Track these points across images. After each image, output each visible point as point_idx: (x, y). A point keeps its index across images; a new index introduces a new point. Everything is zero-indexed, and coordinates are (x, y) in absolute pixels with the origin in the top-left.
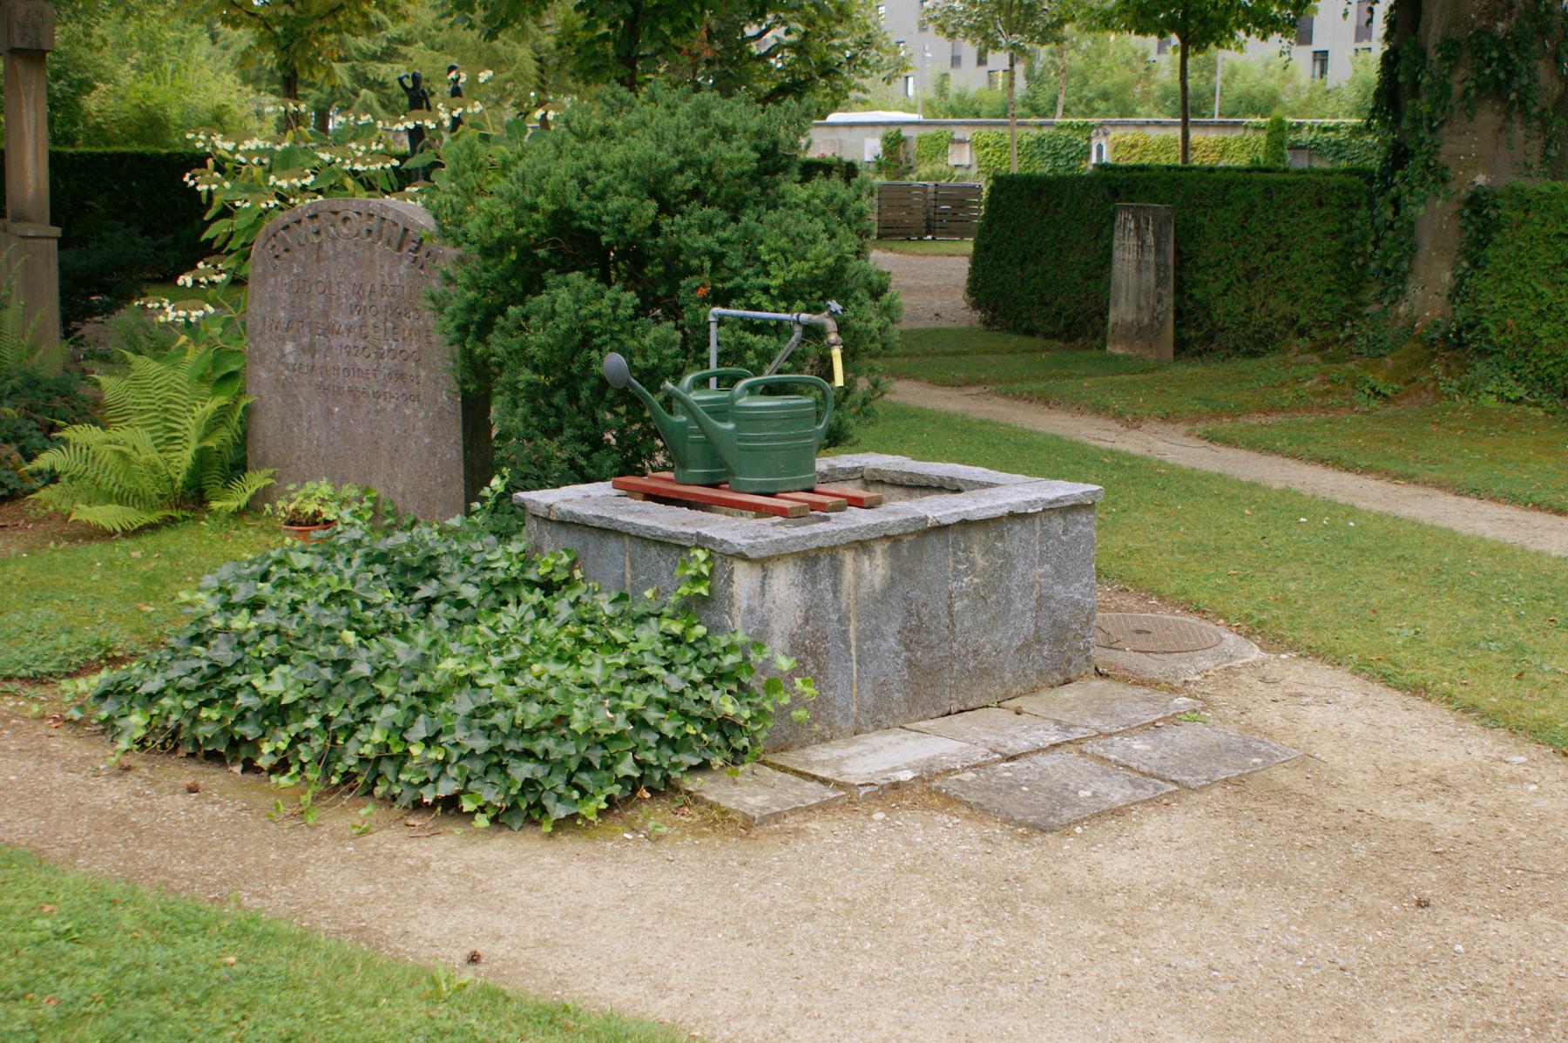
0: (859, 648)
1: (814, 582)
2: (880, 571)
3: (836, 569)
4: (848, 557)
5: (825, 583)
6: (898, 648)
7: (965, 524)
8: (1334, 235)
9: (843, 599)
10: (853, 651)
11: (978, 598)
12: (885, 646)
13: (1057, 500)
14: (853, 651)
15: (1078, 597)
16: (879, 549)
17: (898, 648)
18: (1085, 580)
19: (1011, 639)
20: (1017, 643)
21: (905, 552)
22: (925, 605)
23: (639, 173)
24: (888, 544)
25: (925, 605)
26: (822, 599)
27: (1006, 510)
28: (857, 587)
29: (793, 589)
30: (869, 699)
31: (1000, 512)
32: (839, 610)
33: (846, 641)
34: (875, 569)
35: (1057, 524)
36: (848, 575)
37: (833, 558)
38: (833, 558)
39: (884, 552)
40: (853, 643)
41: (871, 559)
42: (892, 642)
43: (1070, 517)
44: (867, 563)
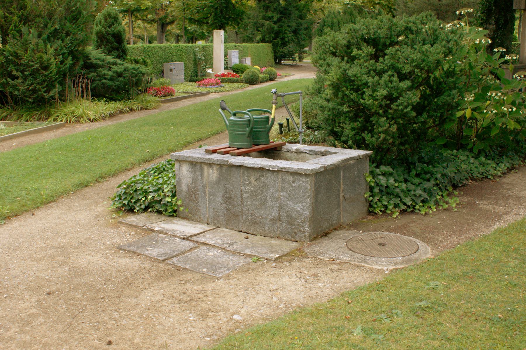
0: (209, 197)
1: (195, 172)
2: (215, 175)
3: (202, 170)
4: (205, 168)
5: (198, 173)
6: (222, 202)
7: (241, 166)
8: (437, 131)
9: (204, 180)
10: (207, 197)
11: (253, 195)
12: (217, 200)
13: (284, 168)
14: (207, 197)
15: (298, 209)
16: (215, 168)
17: (222, 202)
18: (304, 204)
19: (268, 215)
20: (270, 217)
21: (224, 171)
22: (232, 191)
23: (57, 11)
24: (218, 167)
25: (232, 191)
26: (197, 178)
27: (259, 166)
28: (208, 177)
29: (188, 172)
30: (212, 214)
31: (256, 166)
32: (203, 183)
33: (205, 193)
34: (212, 174)
35: (290, 178)
36: (206, 173)
37: (201, 166)
38: (201, 166)
39: (217, 169)
40: (207, 195)
41: (213, 170)
42: (220, 199)
43: (296, 177)
44: (211, 171)
